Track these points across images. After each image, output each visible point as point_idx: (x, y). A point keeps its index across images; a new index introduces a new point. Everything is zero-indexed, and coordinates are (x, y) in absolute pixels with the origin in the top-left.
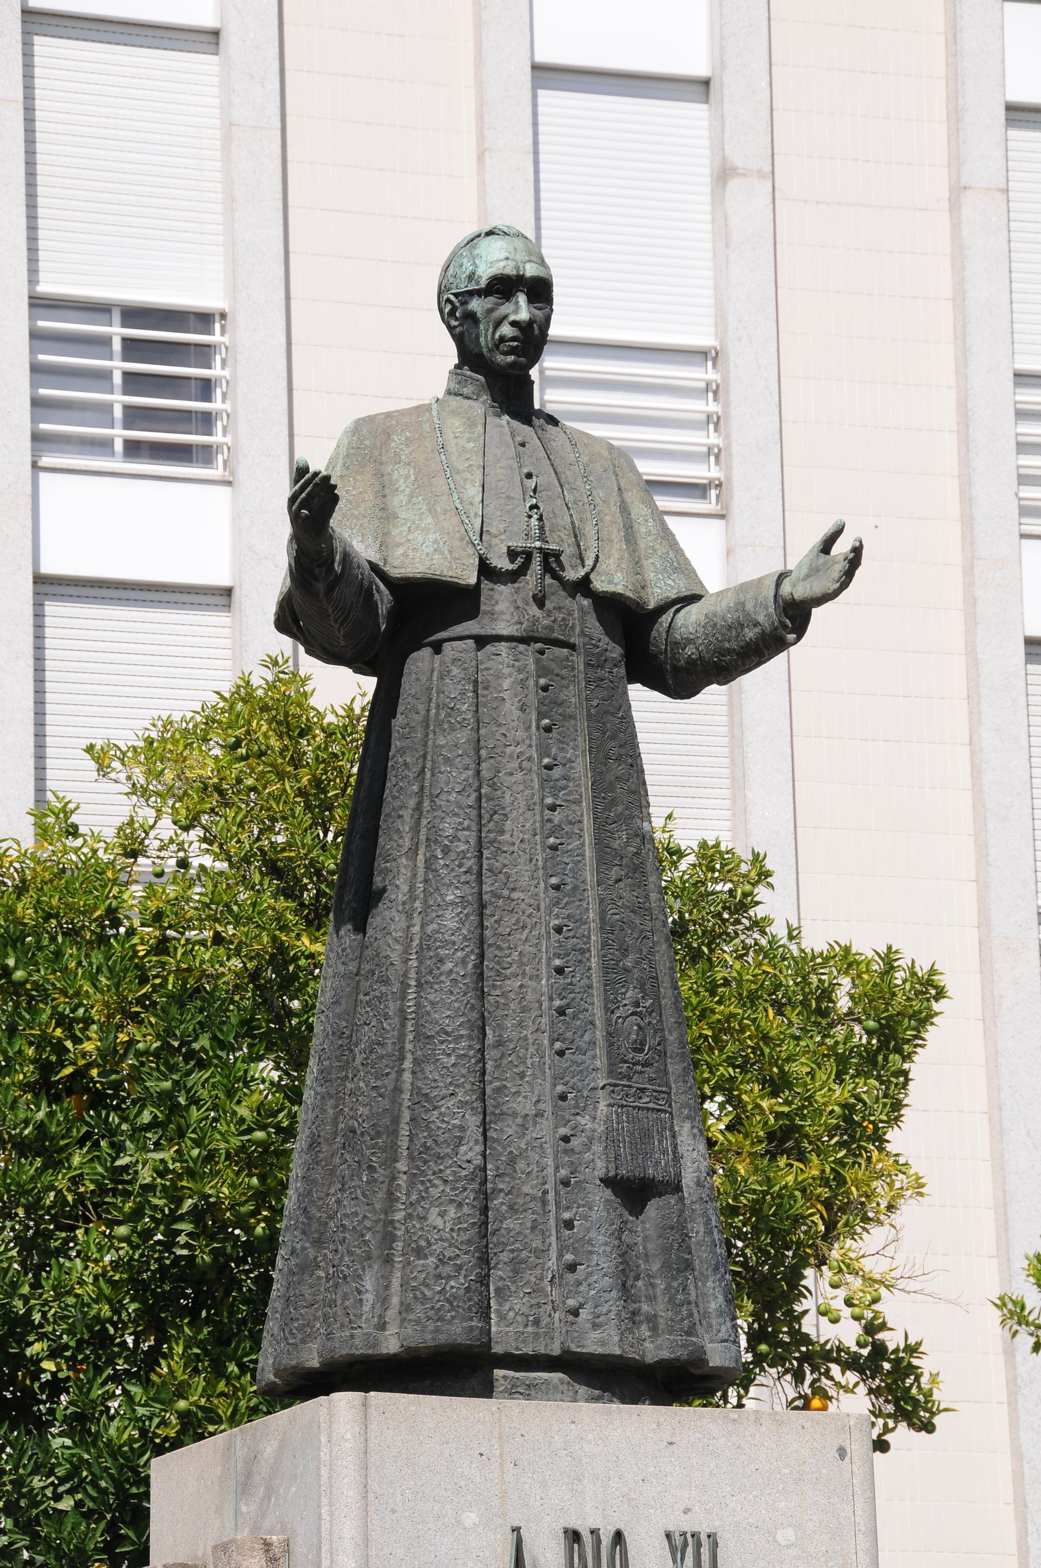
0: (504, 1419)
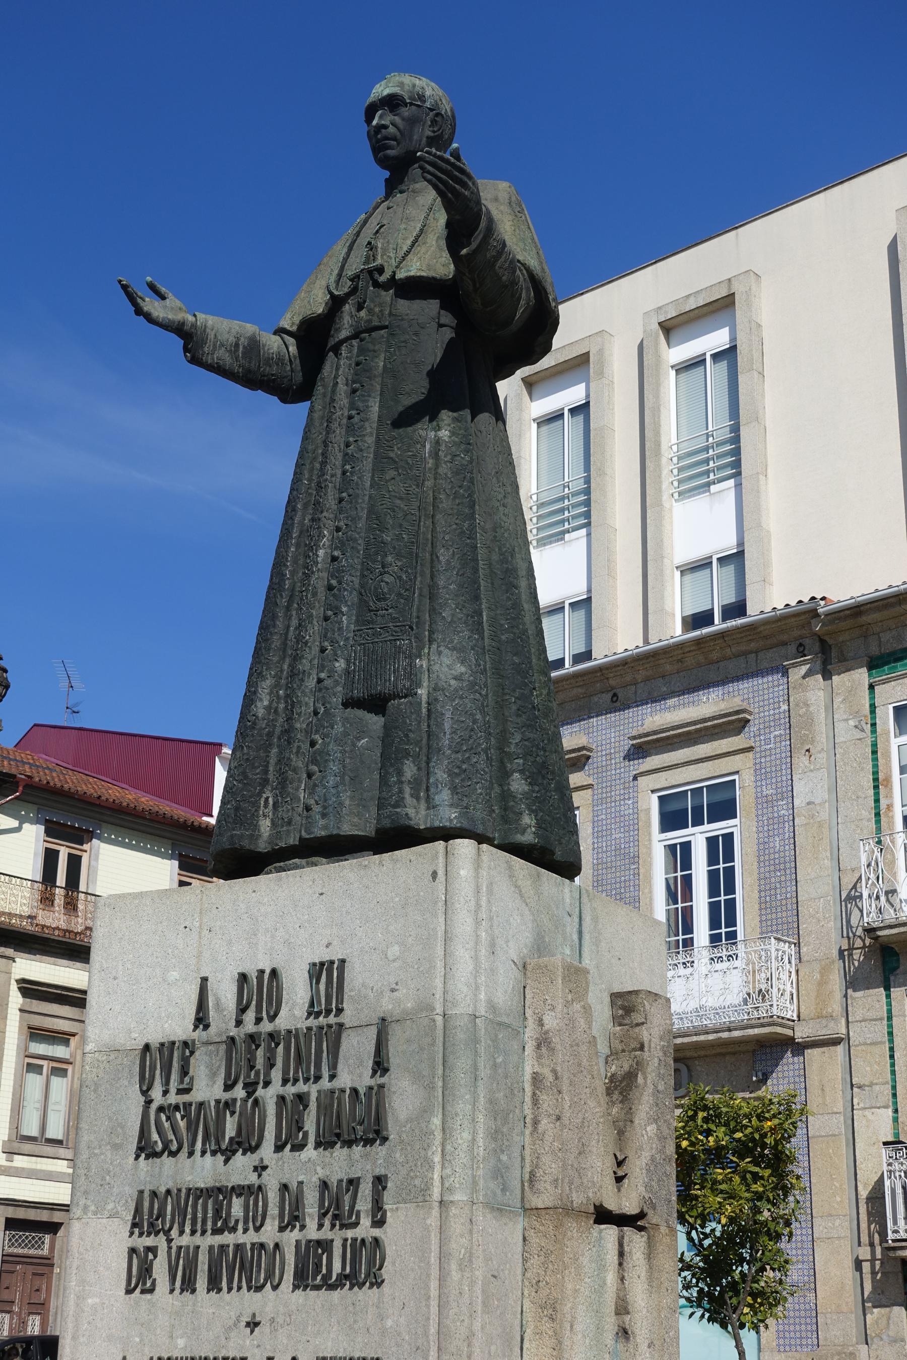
0: (205, 898)
